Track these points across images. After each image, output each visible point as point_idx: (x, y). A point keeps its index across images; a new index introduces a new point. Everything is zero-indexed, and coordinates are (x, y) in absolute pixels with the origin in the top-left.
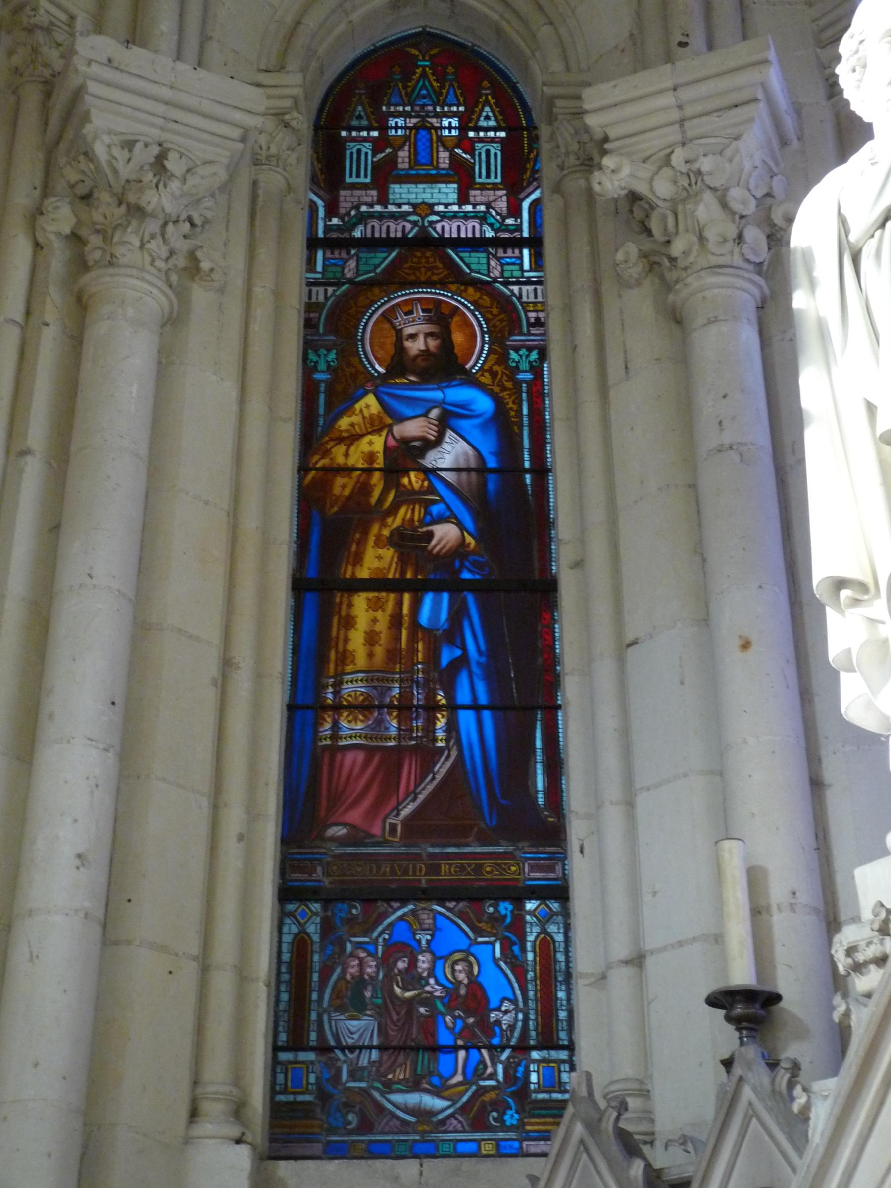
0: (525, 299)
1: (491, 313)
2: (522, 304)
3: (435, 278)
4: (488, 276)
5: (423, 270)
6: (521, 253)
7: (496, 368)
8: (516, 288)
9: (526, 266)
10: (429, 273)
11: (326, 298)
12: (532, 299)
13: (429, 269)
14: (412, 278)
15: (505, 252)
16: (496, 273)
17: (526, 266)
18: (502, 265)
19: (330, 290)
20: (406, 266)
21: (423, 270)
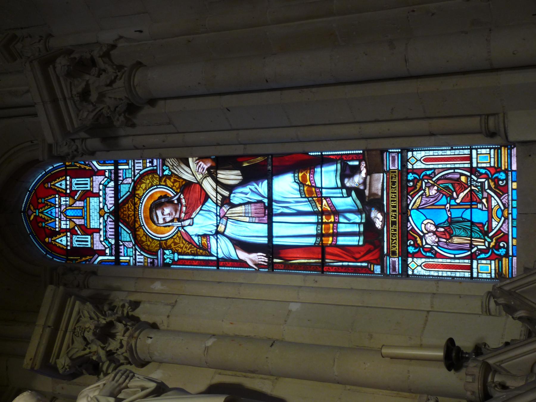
0: (141, 168)
1: (148, 184)
2: (143, 169)
3: (133, 208)
4: (131, 184)
5: (129, 213)
6: (120, 169)
7: (172, 180)
8: (137, 172)
9: (127, 167)
10: (131, 210)
11: (142, 255)
12: (141, 165)
13: (129, 210)
14: (133, 218)
15: (120, 177)
16: (130, 180)
17: (127, 167)
18: (126, 178)
19: (138, 253)
20: (127, 220)
21: (129, 213)
